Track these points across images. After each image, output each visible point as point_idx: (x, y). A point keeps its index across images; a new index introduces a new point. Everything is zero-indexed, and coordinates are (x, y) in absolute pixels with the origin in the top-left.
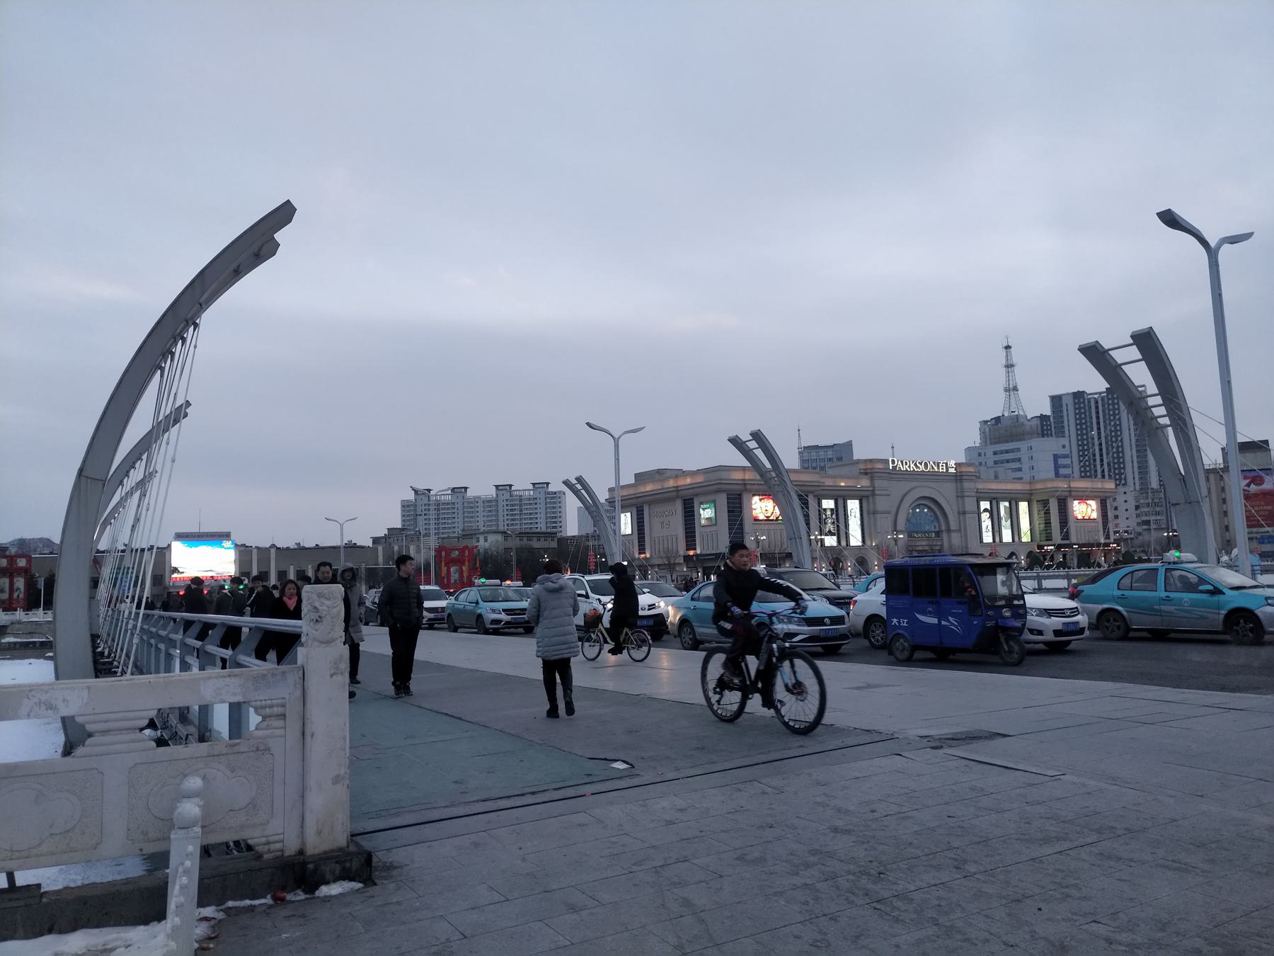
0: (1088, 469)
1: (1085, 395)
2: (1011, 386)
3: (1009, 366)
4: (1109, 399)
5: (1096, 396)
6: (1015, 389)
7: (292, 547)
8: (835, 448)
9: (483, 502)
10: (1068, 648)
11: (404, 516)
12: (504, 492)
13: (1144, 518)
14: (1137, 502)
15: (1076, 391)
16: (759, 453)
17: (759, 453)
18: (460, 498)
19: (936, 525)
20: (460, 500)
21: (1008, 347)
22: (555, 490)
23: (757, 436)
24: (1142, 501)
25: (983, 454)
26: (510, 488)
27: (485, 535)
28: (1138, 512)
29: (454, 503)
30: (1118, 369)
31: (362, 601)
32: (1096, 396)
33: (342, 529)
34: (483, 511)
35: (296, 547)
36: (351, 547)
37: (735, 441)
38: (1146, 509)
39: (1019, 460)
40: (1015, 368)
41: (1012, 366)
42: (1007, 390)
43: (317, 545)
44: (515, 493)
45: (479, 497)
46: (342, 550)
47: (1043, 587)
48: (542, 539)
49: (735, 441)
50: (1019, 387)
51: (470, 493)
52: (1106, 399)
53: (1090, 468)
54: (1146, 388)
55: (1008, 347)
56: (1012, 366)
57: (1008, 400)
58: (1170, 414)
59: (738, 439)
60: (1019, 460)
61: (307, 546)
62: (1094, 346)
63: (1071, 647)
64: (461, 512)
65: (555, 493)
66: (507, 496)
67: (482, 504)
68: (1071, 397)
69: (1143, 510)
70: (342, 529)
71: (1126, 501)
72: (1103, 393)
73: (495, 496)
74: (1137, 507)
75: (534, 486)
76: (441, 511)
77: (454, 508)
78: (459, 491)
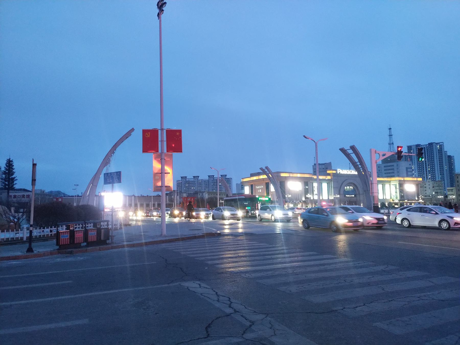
0: (421, 172)
1: (421, 146)
2: (391, 143)
3: (390, 135)
4: (429, 147)
5: (424, 146)
6: (393, 144)
7: (139, 196)
8: (325, 164)
9: (204, 181)
10: (382, 228)
11: (177, 186)
12: (211, 178)
13: (437, 191)
14: (433, 185)
15: (430, 142)
16: (354, 156)
17: (354, 156)
18: (196, 180)
19: (355, 192)
20: (196, 180)
21: (390, 129)
22: (228, 178)
23: (353, 148)
24: (435, 185)
25: (380, 167)
26: (213, 177)
27: (202, 193)
28: (434, 189)
29: (194, 182)
30: (349, 155)
31: (448, 204)
32: (424, 146)
33: (316, 146)
34: (204, 184)
35: (141, 196)
36: (158, 196)
37: (343, 150)
38: (437, 188)
39: (393, 169)
40: (393, 136)
41: (392, 135)
42: (389, 144)
43: (147, 195)
44: (215, 178)
45: (203, 180)
46: (152, 197)
47: (381, 212)
48: (210, 194)
49: (343, 150)
50: (394, 143)
51: (200, 178)
52: (428, 147)
53: (422, 172)
54: (443, 144)
55: (390, 129)
56: (392, 135)
57: (390, 149)
58: (362, 167)
59: (343, 149)
60: (385, 170)
61: (145, 196)
62: (342, 149)
63: (384, 227)
64: (196, 184)
65: (229, 179)
66: (212, 179)
67: (204, 182)
68: (415, 146)
69: (435, 188)
70: (316, 146)
71: (429, 185)
72: (427, 145)
73: (208, 179)
74: (433, 187)
75: (221, 176)
76: (190, 186)
77: (194, 183)
78: (196, 177)
